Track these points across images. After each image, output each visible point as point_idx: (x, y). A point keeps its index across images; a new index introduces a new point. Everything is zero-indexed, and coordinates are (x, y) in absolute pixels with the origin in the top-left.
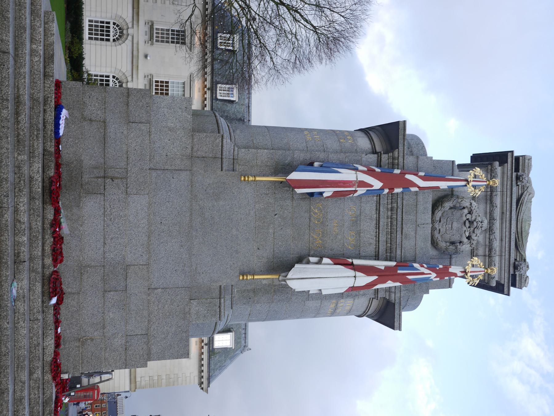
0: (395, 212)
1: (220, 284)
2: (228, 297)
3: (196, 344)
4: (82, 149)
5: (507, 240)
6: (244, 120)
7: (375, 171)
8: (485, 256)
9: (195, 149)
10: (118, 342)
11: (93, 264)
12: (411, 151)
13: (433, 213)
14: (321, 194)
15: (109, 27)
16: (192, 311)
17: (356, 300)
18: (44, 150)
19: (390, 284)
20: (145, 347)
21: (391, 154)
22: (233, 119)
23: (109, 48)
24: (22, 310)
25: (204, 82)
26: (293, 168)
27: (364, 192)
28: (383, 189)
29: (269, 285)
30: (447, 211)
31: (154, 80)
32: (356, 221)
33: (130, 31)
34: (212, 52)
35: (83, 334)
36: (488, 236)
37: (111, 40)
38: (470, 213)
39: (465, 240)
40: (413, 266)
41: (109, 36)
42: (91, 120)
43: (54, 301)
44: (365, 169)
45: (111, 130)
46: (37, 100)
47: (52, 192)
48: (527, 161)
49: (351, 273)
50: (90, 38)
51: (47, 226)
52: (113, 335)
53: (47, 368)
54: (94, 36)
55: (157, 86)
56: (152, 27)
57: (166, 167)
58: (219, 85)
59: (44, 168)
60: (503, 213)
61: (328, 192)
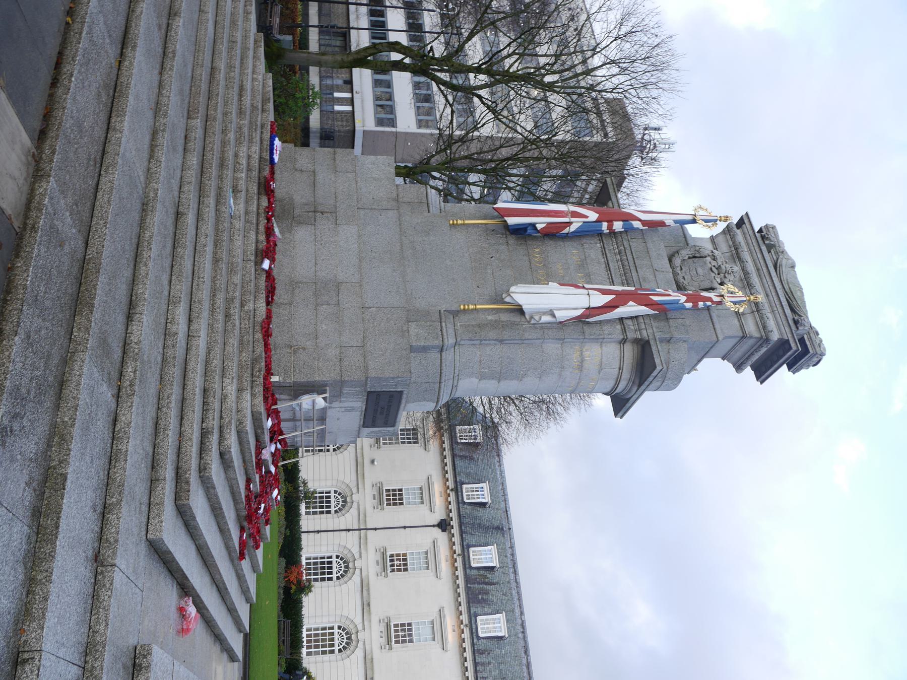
5: (774, 294)
8: (753, 312)
10: (332, 352)
17: (604, 348)
20: (362, 359)
22: (488, 528)
23: (332, 589)
24: (237, 226)
25: (452, 548)
31: (392, 624)
32: (582, 265)
33: (355, 497)
34: (452, 449)
35: (295, 343)
37: (333, 512)
41: (329, 507)
45: (320, 177)
46: (257, 108)
50: (307, 513)
51: (262, 211)
52: (326, 345)
53: (258, 328)
56: (383, 554)
58: (464, 486)
60: (758, 270)
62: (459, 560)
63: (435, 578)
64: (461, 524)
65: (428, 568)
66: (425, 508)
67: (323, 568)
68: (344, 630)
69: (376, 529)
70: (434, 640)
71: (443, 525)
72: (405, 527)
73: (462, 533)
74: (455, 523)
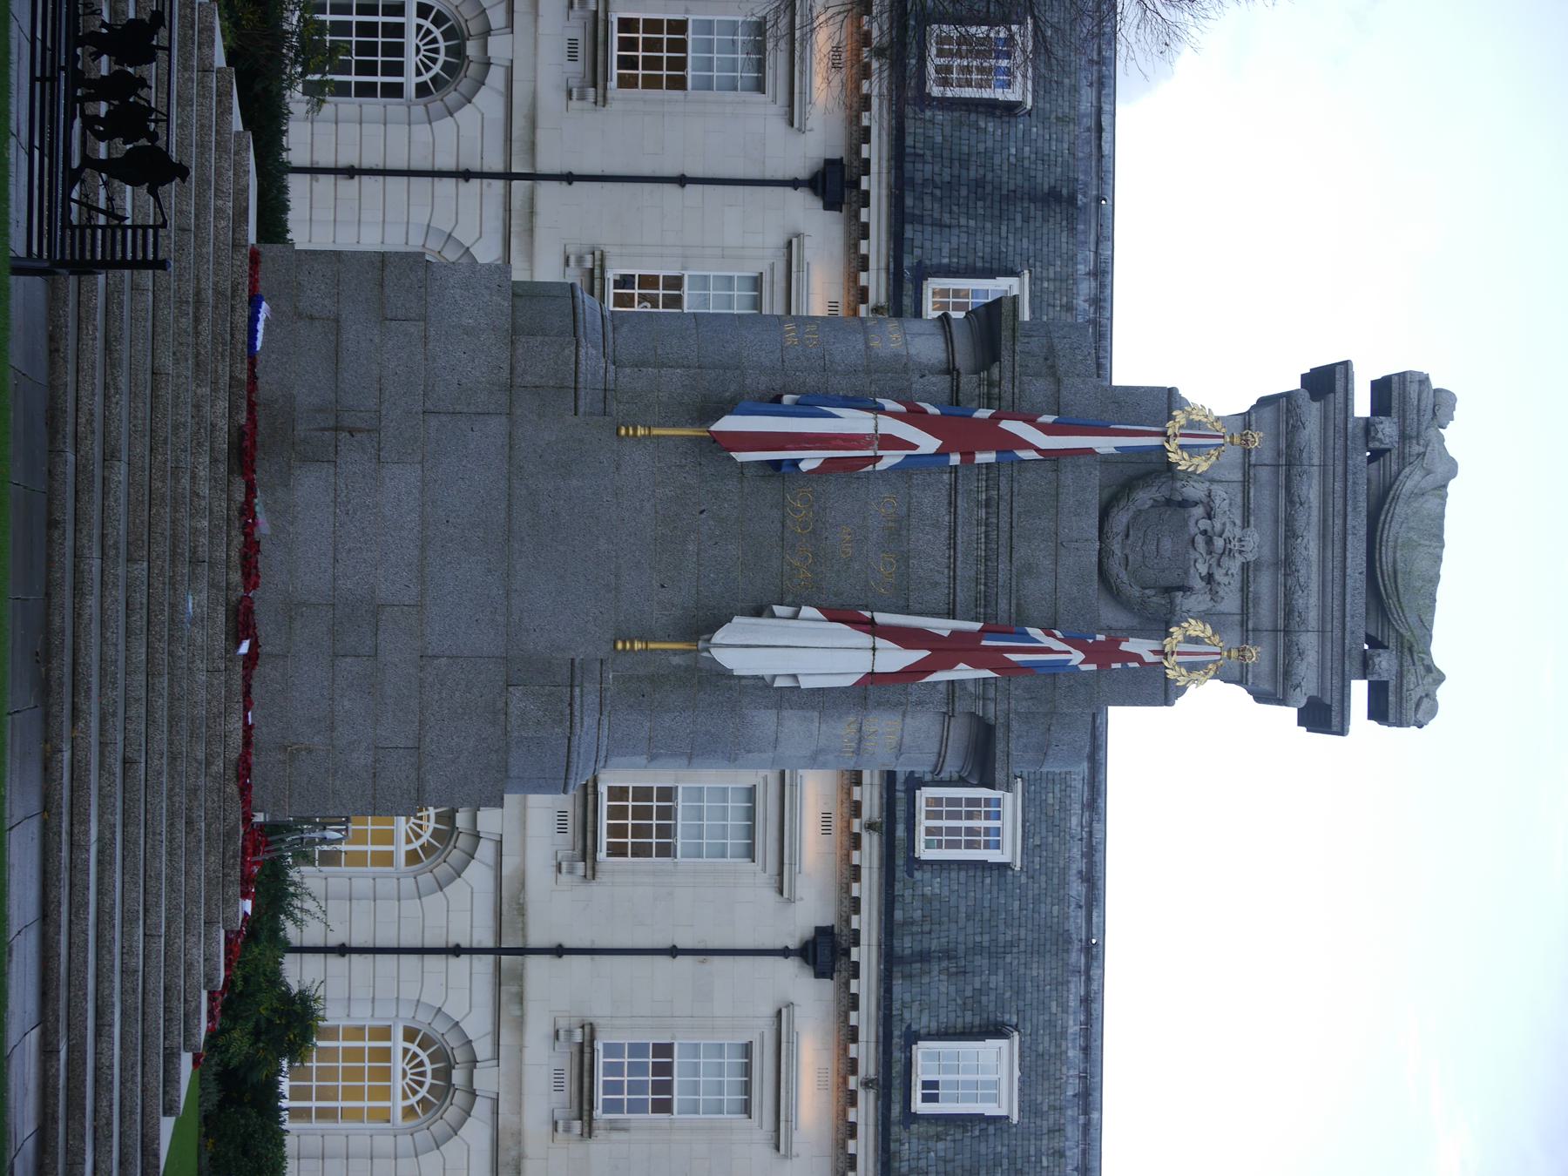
0: (994, 509)
1: (572, 654)
2: (591, 688)
3: (826, 830)
4: (295, 377)
6: (1072, 200)
7: (925, 412)
8: (1275, 630)
9: (519, 370)
11: (313, 599)
12: (1053, 367)
13: (1104, 514)
14: (795, 463)
16: (511, 709)
17: (908, 720)
18: (231, 377)
19: (963, 672)
21: (984, 375)
22: (1011, 197)
25: (844, 1114)
26: (732, 407)
27: (898, 460)
28: (947, 455)
29: (687, 668)
30: (1146, 511)
33: (498, 47)
36: (1281, 579)
38: (1209, 517)
39: (1198, 584)
40: (1027, 634)
42: (312, 318)
43: (244, 648)
44: (902, 408)
47: (243, 455)
49: (864, 639)
55: (627, 44)
57: (458, 408)
59: (233, 409)
61: (811, 460)
63: (768, 1151)
64: (899, 186)
65: (760, 86)
66: (764, 111)
67: (370, 49)
68: (439, 20)
69: (569, 178)
71: (824, 952)
73: (899, 217)
74: (875, 184)
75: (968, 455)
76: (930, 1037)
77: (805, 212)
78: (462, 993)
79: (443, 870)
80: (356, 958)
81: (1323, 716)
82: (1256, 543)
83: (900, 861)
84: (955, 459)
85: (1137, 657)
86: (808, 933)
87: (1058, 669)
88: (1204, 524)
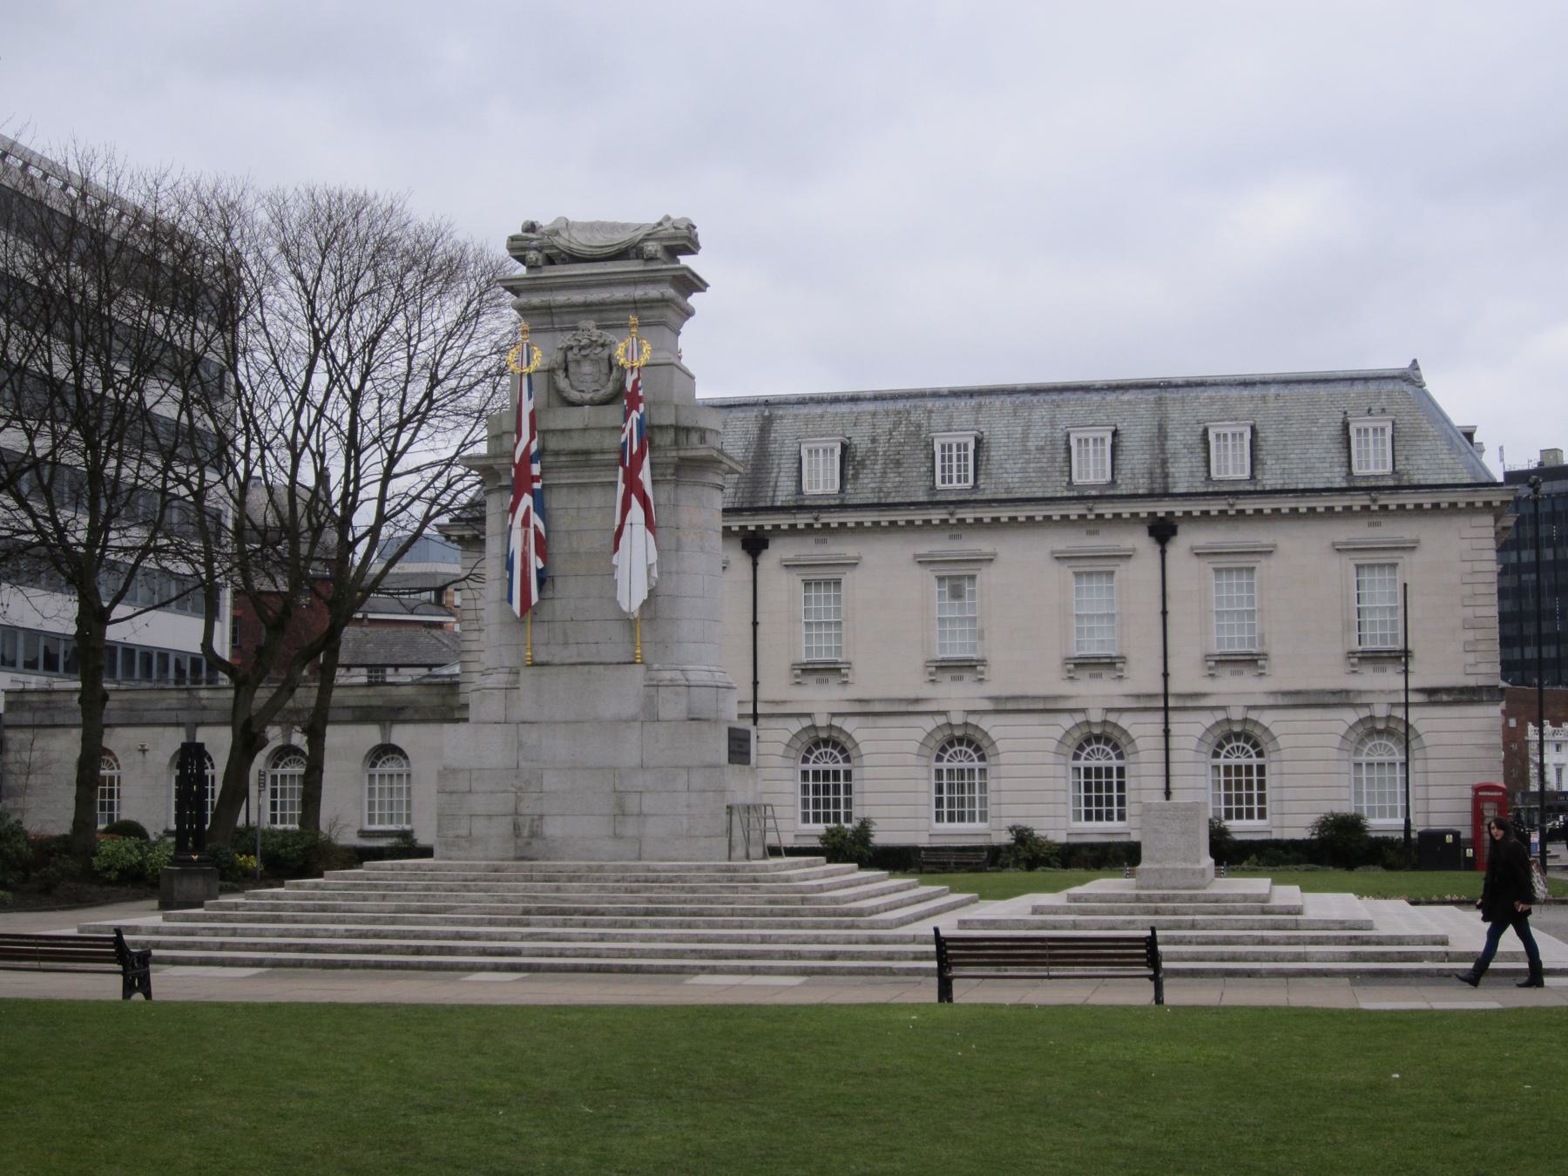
3: (1378, 524)
13: (572, 404)
14: (539, 571)
15: (816, 773)
19: (645, 475)
23: (867, 772)
33: (957, 719)
38: (571, 348)
41: (1249, 769)
48: (516, 244)
49: (627, 529)
54: (842, 810)
61: (536, 563)
62: (825, 518)
63: (1132, 563)
64: (756, 511)
65: (838, 583)
70: (1112, 573)
72: (755, 624)
75: (536, 479)
76: (1209, 472)
77: (1180, 546)
78: (1190, 730)
79: (1124, 740)
80: (1172, 785)
81: (691, 283)
82: (588, 323)
83: (974, 497)
84: (537, 486)
85: (635, 382)
86: (1152, 540)
87: (640, 423)
88: (575, 351)
